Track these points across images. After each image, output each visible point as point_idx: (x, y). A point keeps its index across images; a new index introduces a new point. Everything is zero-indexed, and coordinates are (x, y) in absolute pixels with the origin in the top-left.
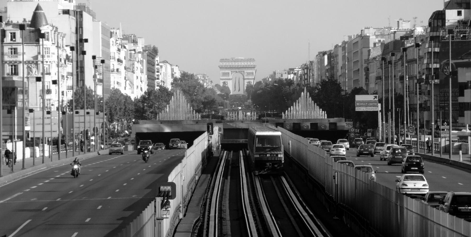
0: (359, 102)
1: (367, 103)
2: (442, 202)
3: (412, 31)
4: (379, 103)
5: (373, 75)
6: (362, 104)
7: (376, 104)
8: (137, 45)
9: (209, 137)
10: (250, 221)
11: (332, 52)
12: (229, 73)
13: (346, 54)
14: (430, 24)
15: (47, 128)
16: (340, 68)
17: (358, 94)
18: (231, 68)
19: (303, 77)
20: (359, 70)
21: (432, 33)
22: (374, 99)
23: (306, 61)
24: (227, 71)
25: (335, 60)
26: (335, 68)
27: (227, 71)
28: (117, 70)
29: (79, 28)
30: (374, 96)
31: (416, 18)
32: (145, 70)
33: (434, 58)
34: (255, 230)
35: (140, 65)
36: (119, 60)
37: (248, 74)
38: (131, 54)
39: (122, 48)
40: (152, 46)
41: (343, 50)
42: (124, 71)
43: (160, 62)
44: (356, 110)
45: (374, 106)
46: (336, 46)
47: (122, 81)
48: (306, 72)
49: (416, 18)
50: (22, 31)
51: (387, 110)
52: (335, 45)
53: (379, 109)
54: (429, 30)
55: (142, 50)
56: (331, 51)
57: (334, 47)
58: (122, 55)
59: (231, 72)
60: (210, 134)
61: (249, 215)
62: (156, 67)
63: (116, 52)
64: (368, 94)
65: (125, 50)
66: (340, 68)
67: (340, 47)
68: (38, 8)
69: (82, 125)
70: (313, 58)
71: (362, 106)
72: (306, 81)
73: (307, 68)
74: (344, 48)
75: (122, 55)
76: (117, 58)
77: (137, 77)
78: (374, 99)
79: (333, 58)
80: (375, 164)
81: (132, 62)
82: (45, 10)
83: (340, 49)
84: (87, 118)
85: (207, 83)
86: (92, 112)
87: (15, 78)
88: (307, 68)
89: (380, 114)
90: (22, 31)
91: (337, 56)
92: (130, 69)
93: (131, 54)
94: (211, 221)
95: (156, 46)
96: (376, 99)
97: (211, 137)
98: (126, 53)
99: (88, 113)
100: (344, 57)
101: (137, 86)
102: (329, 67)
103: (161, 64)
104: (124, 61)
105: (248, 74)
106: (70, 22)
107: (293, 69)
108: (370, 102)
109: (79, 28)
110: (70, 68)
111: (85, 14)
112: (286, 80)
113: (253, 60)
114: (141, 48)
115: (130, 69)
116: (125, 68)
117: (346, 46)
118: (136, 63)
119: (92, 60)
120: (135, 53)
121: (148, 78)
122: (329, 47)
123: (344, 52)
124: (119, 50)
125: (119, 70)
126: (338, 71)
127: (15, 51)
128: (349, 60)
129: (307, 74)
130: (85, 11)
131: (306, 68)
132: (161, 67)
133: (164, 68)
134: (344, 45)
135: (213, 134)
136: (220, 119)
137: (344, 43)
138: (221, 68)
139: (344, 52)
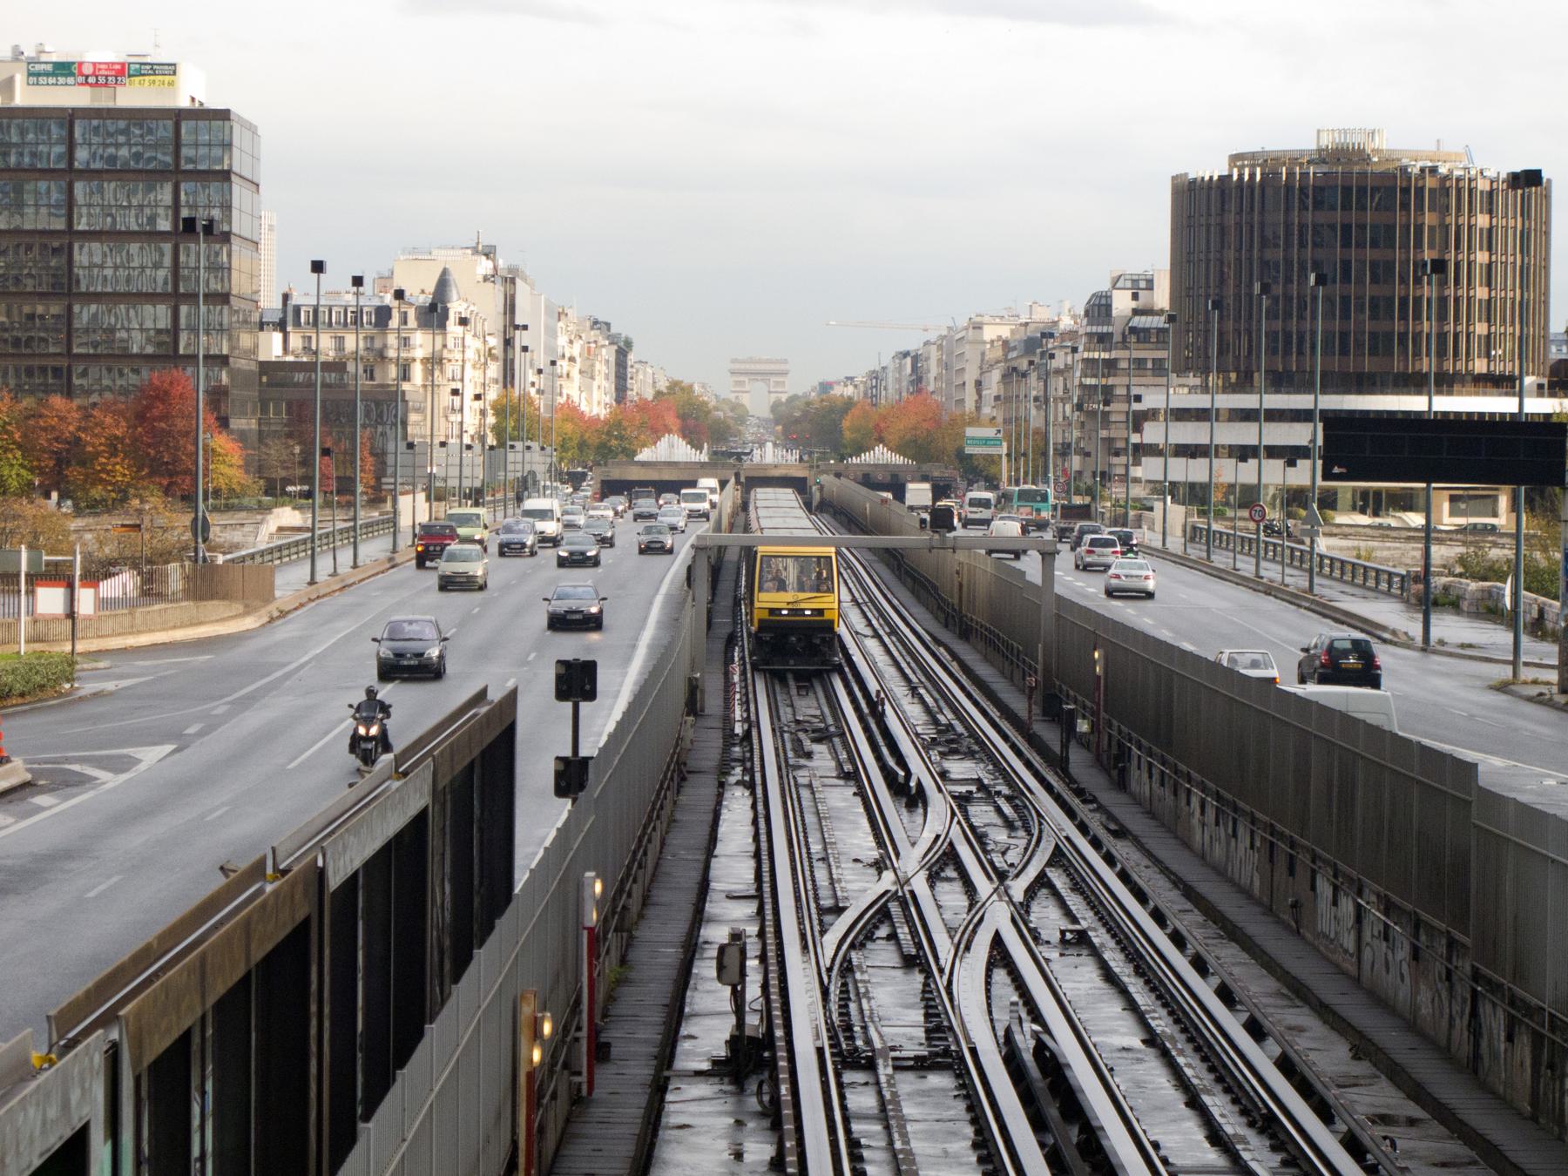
0: (973, 438)
1: (986, 441)
3: (1055, 323)
15: (467, 472)
18: (746, 373)
24: (741, 378)
28: (568, 375)
29: (510, 307)
33: (1446, 383)
35: (604, 368)
36: (572, 359)
37: (777, 383)
38: (589, 348)
46: (927, 343)
53: (1005, 451)
58: (576, 350)
62: (629, 370)
63: (566, 344)
64: (1230, 446)
68: (445, 272)
69: (519, 467)
70: (886, 360)
71: (979, 445)
73: (876, 377)
74: (940, 347)
75: (576, 350)
76: (567, 355)
81: (589, 363)
82: (455, 277)
84: (528, 455)
86: (535, 445)
87: (406, 386)
88: (876, 378)
89: (1004, 460)
91: (927, 359)
92: (588, 374)
93: (589, 348)
95: (630, 336)
98: (582, 347)
99: (529, 448)
100: (940, 361)
103: (636, 366)
105: (777, 383)
106: (495, 295)
107: (851, 379)
108: (987, 440)
109: (510, 307)
111: (518, 281)
112: (842, 395)
113: (785, 362)
118: (597, 363)
119: (842, 378)
122: (913, 344)
124: (571, 342)
127: (406, 342)
133: (641, 372)
136: (1094, 499)
137: (943, 338)
138: (733, 373)
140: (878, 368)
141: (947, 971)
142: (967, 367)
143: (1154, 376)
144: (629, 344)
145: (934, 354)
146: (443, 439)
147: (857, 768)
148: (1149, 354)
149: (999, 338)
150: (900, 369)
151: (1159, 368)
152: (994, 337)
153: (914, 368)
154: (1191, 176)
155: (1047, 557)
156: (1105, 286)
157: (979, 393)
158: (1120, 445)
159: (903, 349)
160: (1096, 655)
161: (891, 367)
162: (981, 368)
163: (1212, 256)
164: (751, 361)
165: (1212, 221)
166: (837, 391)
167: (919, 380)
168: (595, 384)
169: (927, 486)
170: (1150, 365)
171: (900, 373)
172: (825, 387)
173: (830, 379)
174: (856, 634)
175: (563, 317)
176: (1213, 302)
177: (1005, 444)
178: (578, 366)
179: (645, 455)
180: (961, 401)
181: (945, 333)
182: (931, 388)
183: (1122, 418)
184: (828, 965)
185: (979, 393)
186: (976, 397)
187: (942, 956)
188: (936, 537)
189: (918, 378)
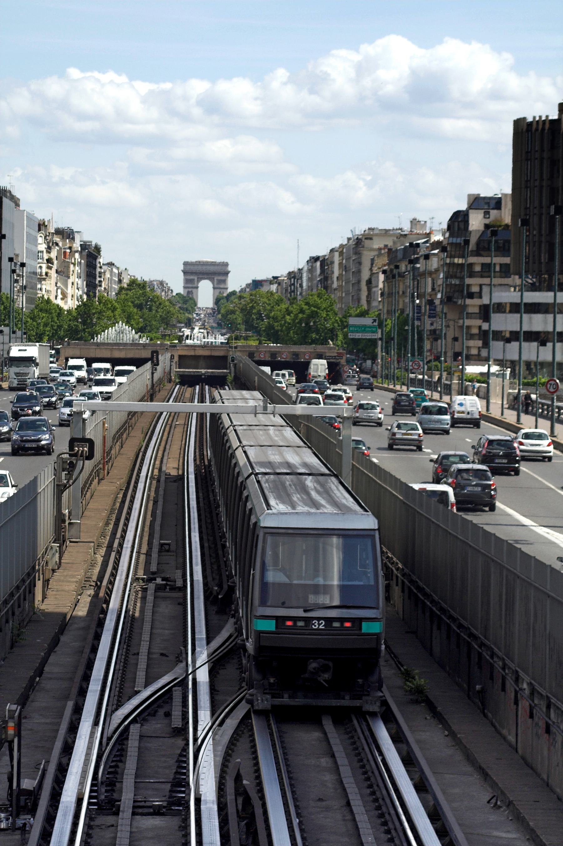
0: (353, 326)
1: (363, 328)
4: (379, 328)
7: (374, 329)
8: (74, 241)
9: (153, 368)
10: (190, 484)
11: (326, 257)
12: (194, 280)
13: (344, 261)
14: (449, 227)
19: (289, 288)
21: (451, 239)
23: (293, 268)
24: (192, 277)
25: (330, 269)
26: (329, 279)
27: (192, 277)
31: (433, 218)
32: (83, 275)
34: (195, 497)
38: (65, 252)
39: (53, 245)
40: (93, 244)
41: (340, 256)
42: (56, 275)
43: (103, 264)
44: (349, 337)
45: (373, 332)
46: (332, 251)
47: (53, 289)
48: (292, 282)
49: (433, 218)
51: (388, 340)
52: (331, 248)
53: (380, 336)
54: (447, 235)
55: (79, 249)
56: (325, 256)
57: (329, 251)
59: (198, 278)
60: (155, 365)
61: (190, 476)
65: (57, 248)
67: (337, 251)
71: (357, 332)
72: (293, 294)
74: (341, 254)
77: (73, 283)
78: (373, 323)
80: (518, 351)
83: (337, 254)
85: (166, 292)
91: (332, 263)
92: (63, 273)
94: (141, 482)
95: (99, 243)
96: (375, 324)
97: (156, 370)
100: (340, 264)
101: (72, 296)
102: (322, 277)
103: (105, 268)
104: (55, 262)
108: (365, 326)
114: (78, 245)
115: (63, 273)
116: (57, 272)
117: (344, 250)
120: (71, 252)
122: (323, 251)
123: (341, 258)
125: (49, 274)
128: (347, 269)
129: (294, 284)
130: (6, 197)
131: (293, 277)
134: (341, 250)
135: (158, 365)
137: (342, 246)
139: (341, 258)
141: (199, 741)
143: (501, 277)
144: (98, 249)
145: (337, 258)
146: (456, 343)
147: (185, 587)
148: (499, 260)
149: (386, 246)
150: (311, 270)
151: (505, 271)
152: (382, 246)
154: (530, 119)
156: (463, 206)
157: (369, 290)
158: (475, 331)
159: (314, 255)
161: (306, 269)
163: (544, 184)
165: (545, 155)
168: (70, 281)
169: (324, 362)
170: (498, 268)
175: (43, 228)
176: (522, 221)
177: (380, 331)
178: (55, 267)
179: (100, 339)
181: (345, 242)
182: (335, 285)
183: (477, 310)
184: (109, 735)
187: (200, 728)
189: (325, 278)
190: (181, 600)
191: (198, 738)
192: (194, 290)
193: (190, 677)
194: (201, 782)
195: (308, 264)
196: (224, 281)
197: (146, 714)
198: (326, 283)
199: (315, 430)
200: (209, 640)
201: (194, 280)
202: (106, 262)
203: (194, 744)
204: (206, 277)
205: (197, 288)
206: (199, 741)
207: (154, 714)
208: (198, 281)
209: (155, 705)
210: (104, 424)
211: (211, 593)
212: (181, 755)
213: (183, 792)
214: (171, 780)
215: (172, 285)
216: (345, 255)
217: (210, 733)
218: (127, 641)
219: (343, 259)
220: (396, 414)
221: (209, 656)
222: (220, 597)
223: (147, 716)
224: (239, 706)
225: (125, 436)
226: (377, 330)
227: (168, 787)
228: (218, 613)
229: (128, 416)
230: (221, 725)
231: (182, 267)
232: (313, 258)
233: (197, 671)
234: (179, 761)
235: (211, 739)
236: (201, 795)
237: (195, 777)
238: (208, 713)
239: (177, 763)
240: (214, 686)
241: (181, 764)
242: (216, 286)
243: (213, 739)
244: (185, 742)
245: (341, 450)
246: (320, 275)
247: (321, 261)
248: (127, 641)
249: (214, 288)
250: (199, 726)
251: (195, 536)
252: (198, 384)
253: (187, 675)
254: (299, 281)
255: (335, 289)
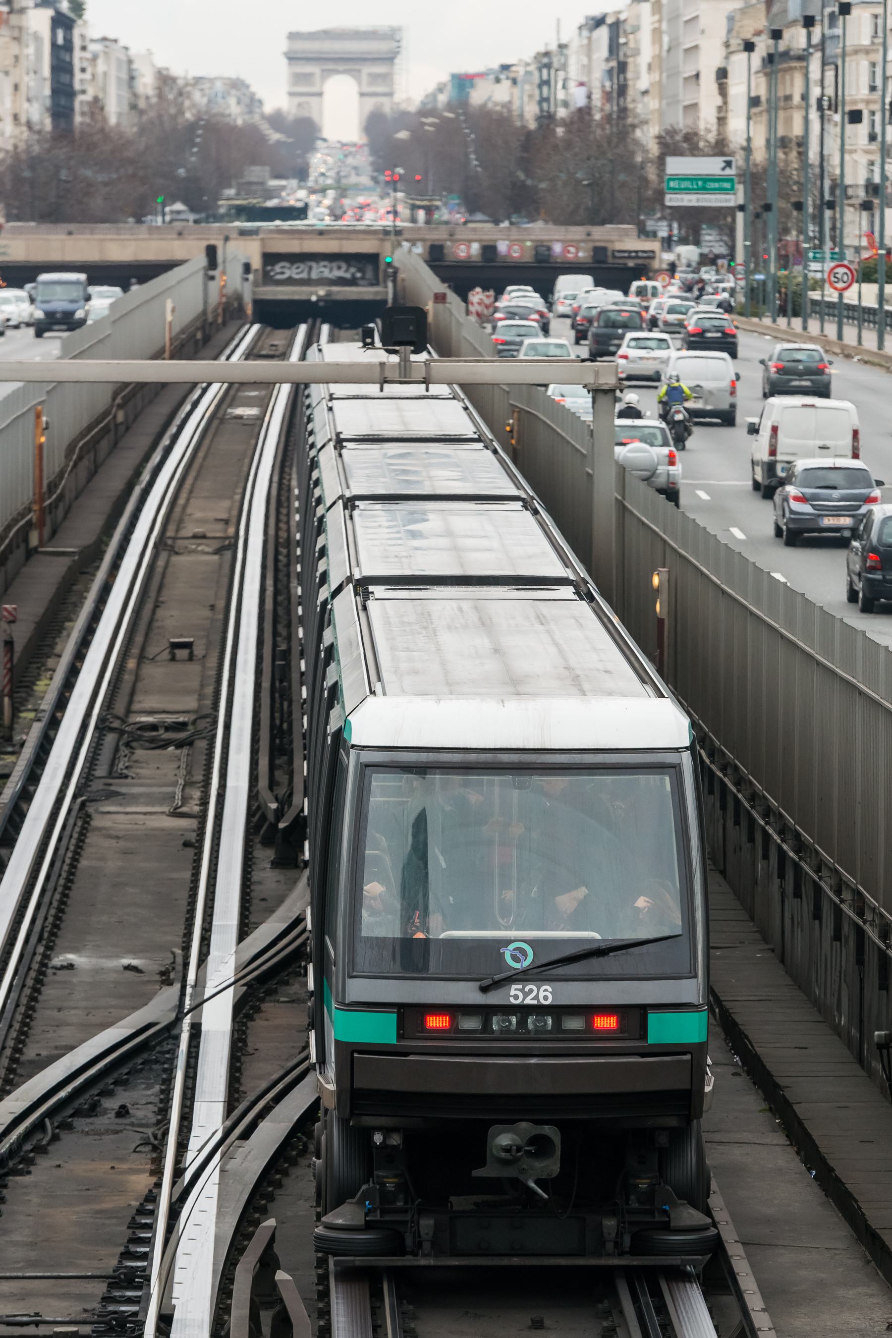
1: (703, 183)
2: (241, 309)
5: (738, 90)
6: (685, 184)
7: (727, 185)
16: (644, 69)
17: (677, 152)
20: (697, 76)
22: (723, 169)
26: (630, 68)
30: (725, 161)
50: (194, 831)
56: (619, 12)
59: (323, 71)
66: (644, 69)
71: (687, 191)
78: (723, 169)
79: (626, 34)
90: (194, 831)
91: (636, 29)
96: (728, 171)
110: (290, 448)
121: (55, 92)
123: (657, 17)
126: (637, 78)
132: (95, 58)
139: (657, 17)
140: (553, 47)
141: (188, 1176)
142: (702, 42)
153: (614, 47)
155: (601, 398)
157: (723, 90)
159: (597, 12)
160: (656, 581)
161: (575, 45)
162: (727, 45)
164: (326, 35)
166: (478, 96)
167: (622, 67)
171: (589, 56)
172: (463, 82)
173: (472, 69)
174: (199, 545)
180: (693, 107)
185: (723, 90)
186: (719, 101)
187: (194, 1144)
188: (395, 359)
190: (193, 837)
191: (186, 1169)
192: (314, 100)
193: (187, 1020)
194: (178, 1275)
195: (580, 34)
196: (387, 78)
197: (70, 1111)
198: (621, 77)
199: (545, 423)
200: (244, 931)
201: (311, 75)
202: (97, 35)
203: (174, 1183)
204: (341, 67)
205: (320, 94)
206: (188, 1176)
207: (93, 1110)
208: (323, 79)
209: (95, 1091)
210: (38, 416)
211: (264, 817)
212: (141, 1211)
213: (130, 1301)
214: (110, 1272)
215: (259, 89)
216: (665, 11)
217: (217, 1156)
218: (46, 935)
219: (660, 21)
220: (47, 334)
221: (238, 970)
222: (281, 825)
223: (72, 1116)
224: (296, 1090)
225: (104, 445)
226: (732, 188)
227: (101, 1288)
228: (276, 864)
229: (114, 399)
230: (246, 1135)
231: (284, 45)
232: (593, 19)
233: (205, 1005)
234: (134, 1225)
235: (218, 1169)
236: (174, 1306)
237: (166, 1266)
238: (219, 1109)
239: (130, 1231)
240: (244, 1041)
241: (137, 1231)
242: (366, 89)
243: (222, 1171)
244: (154, 1180)
245: (593, 470)
246: (607, 60)
247: (611, 26)
248: (46, 935)
249: (362, 95)
250: (192, 1139)
251: (245, 682)
252: (305, 322)
253: (178, 1020)
254: (561, 74)
255: (645, 93)
